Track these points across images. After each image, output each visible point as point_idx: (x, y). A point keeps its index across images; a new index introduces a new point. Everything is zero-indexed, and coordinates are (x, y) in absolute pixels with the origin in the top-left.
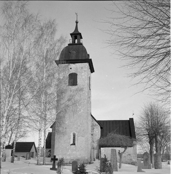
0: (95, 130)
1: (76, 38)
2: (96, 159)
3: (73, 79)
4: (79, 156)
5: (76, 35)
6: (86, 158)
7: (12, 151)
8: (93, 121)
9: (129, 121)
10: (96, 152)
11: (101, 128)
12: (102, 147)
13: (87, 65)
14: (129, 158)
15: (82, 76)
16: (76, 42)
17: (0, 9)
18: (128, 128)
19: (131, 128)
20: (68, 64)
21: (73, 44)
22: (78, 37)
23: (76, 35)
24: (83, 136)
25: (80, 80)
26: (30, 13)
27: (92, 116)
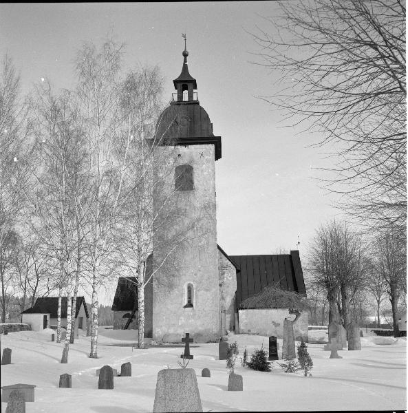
0: (226, 275)
1: (185, 88)
2: (228, 331)
3: (185, 178)
4: (200, 328)
5: (185, 83)
6: (215, 331)
7: (45, 317)
8: (221, 258)
9: (290, 256)
10: (228, 318)
11: (238, 271)
12: (242, 309)
13: (212, 147)
15: (202, 171)
16: (186, 98)
18: (289, 271)
19: (296, 273)
20: (303, 270)
21: (180, 102)
22: (190, 86)
23: (185, 83)
24: (207, 290)
25: (198, 178)
27: (219, 248)
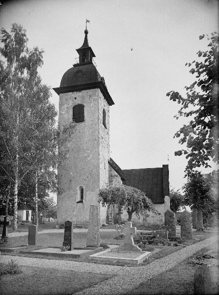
3: (78, 114)
5: (86, 52)
14: (158, 219)
17: (0, 32)
23: (86, 52)
26: (189, 124)
